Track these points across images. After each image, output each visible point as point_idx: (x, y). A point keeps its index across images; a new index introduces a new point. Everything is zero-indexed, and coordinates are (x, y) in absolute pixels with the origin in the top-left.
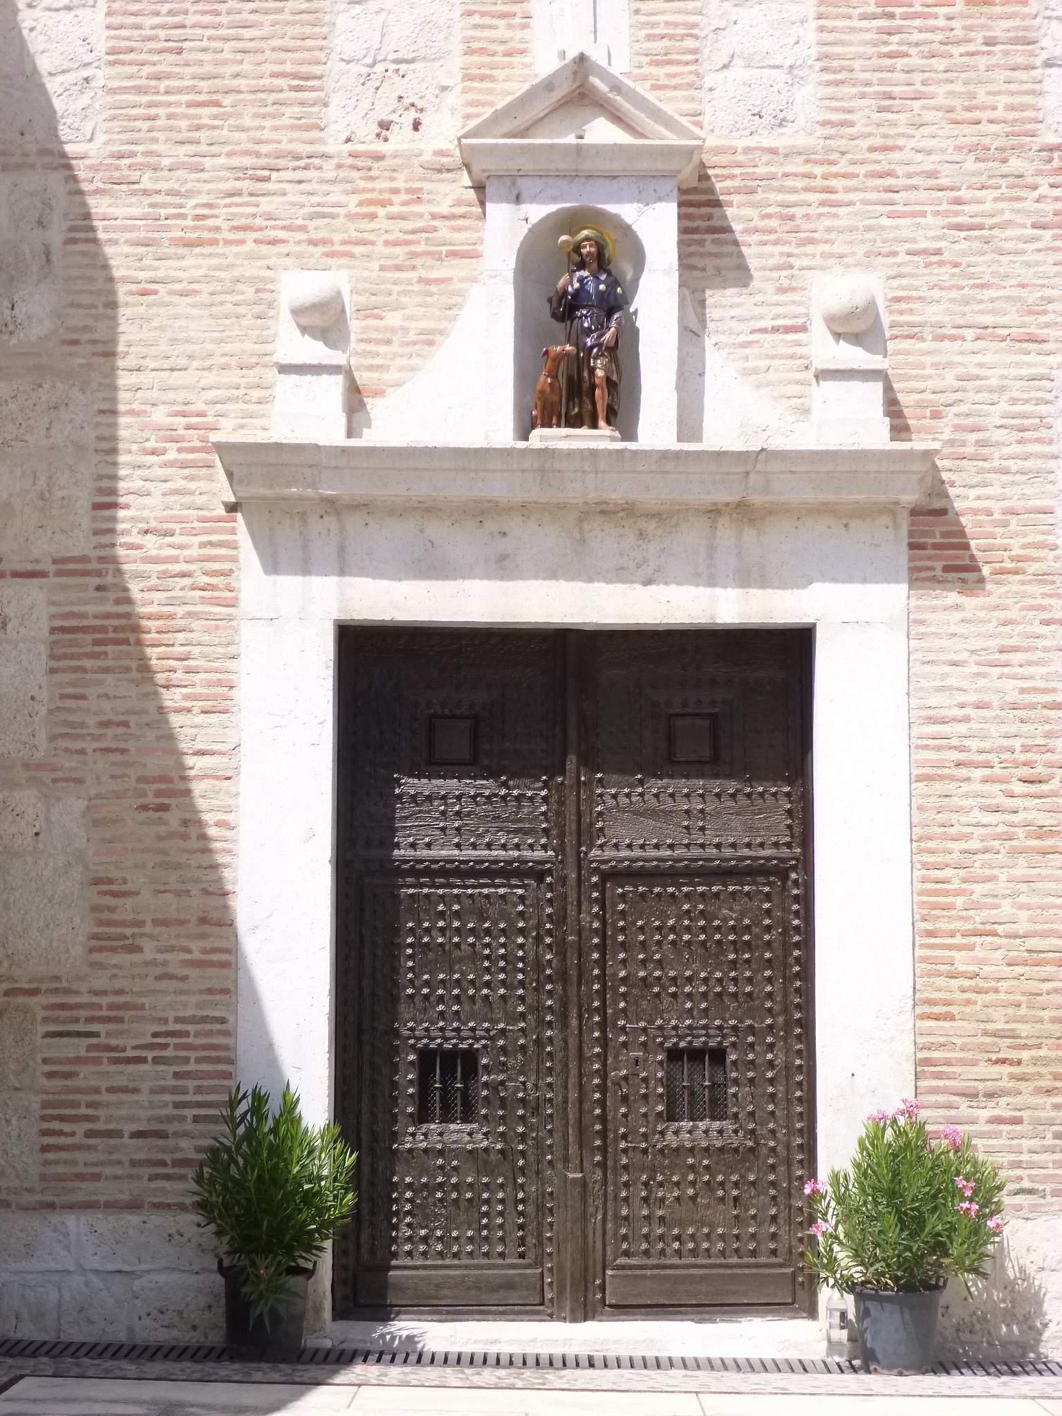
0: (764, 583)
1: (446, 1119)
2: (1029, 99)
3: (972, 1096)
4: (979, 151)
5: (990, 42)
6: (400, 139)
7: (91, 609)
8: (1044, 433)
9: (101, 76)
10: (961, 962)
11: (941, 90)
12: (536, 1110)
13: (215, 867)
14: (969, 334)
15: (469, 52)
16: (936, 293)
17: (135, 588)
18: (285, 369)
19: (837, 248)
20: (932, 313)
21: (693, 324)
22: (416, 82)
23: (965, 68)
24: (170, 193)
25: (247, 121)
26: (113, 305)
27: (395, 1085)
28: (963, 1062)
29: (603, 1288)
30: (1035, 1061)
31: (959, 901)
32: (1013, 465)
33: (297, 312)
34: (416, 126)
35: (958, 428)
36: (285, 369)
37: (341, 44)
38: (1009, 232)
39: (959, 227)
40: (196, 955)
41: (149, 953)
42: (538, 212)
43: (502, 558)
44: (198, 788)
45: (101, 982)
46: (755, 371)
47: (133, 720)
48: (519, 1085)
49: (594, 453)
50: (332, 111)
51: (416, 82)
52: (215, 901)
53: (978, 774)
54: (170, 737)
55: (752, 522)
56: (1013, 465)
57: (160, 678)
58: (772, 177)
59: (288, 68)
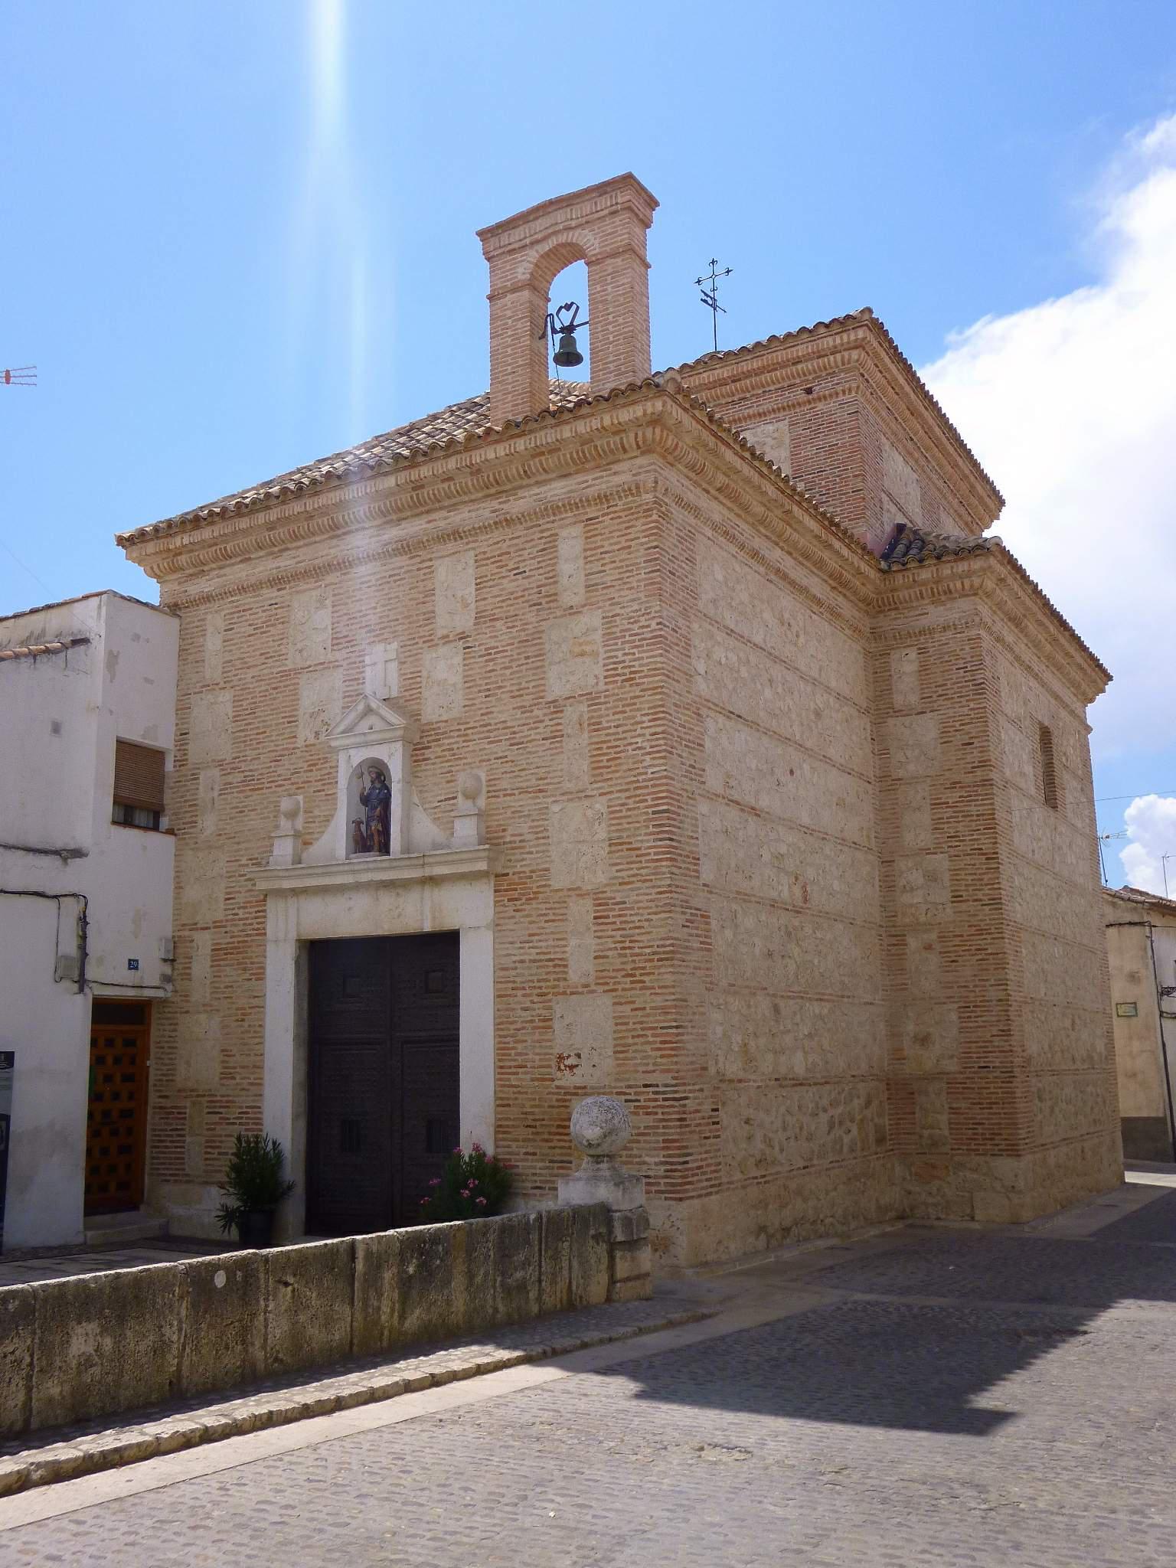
14: (516, 792)
31: (513, 1052)
35: (512, 835)
41: (238, 1081)
58: (446, 733)
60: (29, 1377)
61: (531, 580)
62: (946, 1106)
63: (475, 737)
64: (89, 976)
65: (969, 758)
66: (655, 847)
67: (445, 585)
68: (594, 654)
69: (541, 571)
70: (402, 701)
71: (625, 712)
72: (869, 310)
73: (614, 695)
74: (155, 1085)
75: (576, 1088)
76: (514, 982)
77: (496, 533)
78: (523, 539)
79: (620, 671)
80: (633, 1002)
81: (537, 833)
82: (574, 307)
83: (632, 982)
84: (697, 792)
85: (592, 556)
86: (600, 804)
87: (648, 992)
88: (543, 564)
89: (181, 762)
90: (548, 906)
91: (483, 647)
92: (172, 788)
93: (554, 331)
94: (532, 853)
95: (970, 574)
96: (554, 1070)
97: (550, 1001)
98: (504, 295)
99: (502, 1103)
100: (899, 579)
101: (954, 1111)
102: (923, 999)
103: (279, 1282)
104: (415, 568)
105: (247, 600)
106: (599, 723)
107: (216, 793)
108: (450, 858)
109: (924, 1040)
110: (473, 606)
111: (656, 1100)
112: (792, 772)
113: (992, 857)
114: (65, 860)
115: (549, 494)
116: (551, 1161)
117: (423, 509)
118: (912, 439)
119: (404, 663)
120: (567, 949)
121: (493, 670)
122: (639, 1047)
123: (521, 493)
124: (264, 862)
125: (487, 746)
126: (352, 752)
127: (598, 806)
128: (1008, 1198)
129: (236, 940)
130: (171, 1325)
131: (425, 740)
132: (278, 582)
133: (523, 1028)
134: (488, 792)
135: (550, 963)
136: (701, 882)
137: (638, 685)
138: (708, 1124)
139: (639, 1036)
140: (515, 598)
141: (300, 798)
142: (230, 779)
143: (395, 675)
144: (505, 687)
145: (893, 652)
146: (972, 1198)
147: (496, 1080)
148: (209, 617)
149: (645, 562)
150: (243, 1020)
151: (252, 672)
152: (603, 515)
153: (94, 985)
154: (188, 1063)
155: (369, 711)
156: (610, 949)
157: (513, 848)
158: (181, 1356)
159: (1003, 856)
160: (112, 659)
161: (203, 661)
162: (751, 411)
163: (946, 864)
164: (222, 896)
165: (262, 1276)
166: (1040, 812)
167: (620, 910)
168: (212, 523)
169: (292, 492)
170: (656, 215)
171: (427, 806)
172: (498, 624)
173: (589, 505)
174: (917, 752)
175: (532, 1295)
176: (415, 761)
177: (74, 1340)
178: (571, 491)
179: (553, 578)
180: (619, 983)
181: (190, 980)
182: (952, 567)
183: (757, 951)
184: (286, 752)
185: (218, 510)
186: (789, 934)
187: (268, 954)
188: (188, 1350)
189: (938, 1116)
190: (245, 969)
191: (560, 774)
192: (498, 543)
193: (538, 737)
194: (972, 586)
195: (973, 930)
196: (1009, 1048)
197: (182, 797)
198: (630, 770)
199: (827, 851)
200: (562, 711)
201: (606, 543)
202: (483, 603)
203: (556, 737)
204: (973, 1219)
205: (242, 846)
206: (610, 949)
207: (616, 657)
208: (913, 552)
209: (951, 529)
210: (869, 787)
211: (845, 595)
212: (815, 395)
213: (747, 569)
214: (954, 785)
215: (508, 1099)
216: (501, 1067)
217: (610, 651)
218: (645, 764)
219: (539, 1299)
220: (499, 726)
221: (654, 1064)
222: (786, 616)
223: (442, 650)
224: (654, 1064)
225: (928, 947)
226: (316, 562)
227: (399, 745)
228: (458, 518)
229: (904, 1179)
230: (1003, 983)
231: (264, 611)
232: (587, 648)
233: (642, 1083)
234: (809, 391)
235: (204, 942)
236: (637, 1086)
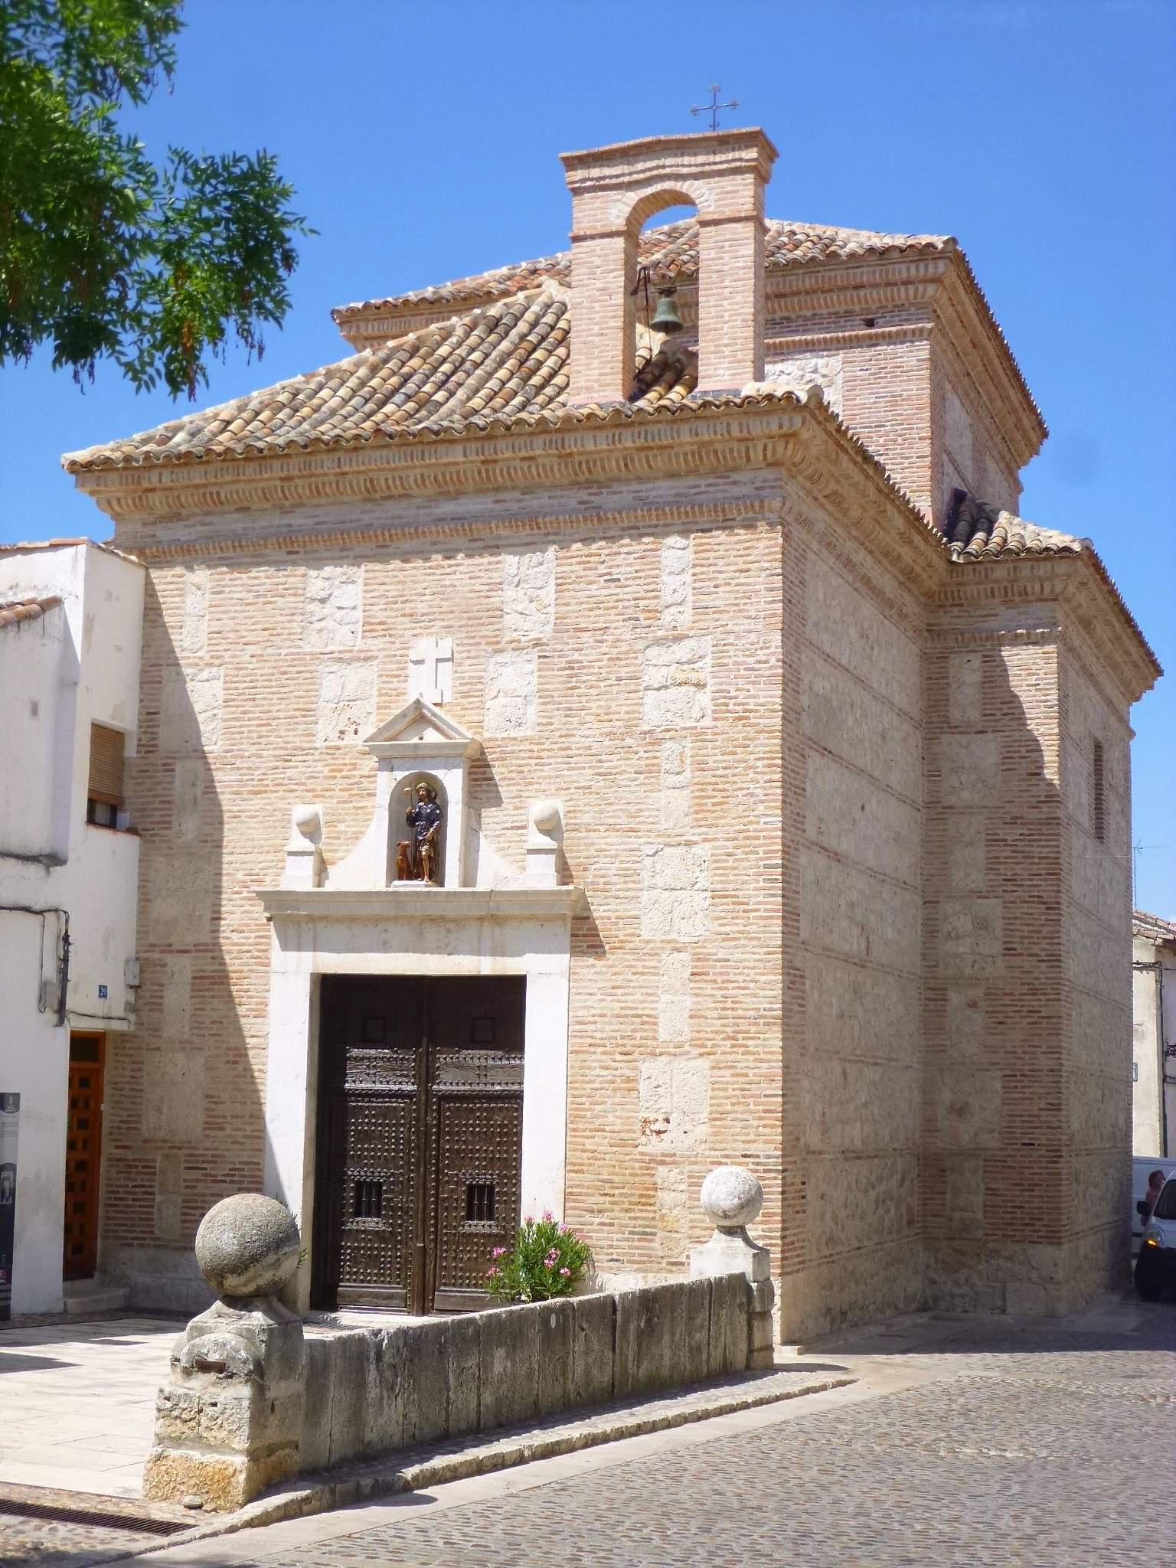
0: (503, 954)
1: (481, 1219)
2: (636, 708)
3: (592, 1211)
4: (611, 735)
5: (619, 679)
6: (349, 740)
7: (209, 968)
8: (636, 878)
9: (220, 712)
10: (589, 1144)
11: (594, 705)
12: (406, 1213)
13: (257, 1091)
14: (602, 828)
15: (380, 695)
16: (587, 808)
17: (227, 957)
18: (291, 854)
19: (543, 787)
20: (586, 818)
21: (475, 825)
22: (355, 712)
23: (607, 693)
24: (249, 769)
25: (283, 733)
26: (221, 823)
27: (344, 1198)
28: (587, 1194)
29: (433, 1300)
30: (621, 1195)
31: (588, 1114)
32: (621, 894)
33: (299, 825)
34: (356, 732)
35: (595, 876)
36: (291, 854)
37: (326, 694)
38: (624, 776)
39: (600, 774)
40: (248, 1133)
41: (228, 1131)
42: (400, 775)
43: (385, 943)
44: (251, 1053)
45: (208, 1144)
46: (502, 849)
47: (225, 1021)
48: (400, 1200)
49: (417, 893)
50: (320, 727)
51: (355, 712)
52: (256, 1107)
53: (600, 1050)
54: (239, 1029)
55: (499, 924)
56: (621, 894)
57: (237, 1000)
58: (513, 752)
59: (301, 706)
62: (982, 1187)
67: (516, 579)
69: (641, 582)
74: (111, 1134)
75: (663, 1155)
76: (592, 1037)
79: (731, 707)
85: (703, 573)
89: (148, 747)
92: (133, 778)
96: (639, 1133)
99: (572, 1167)
101: (991, 1192)
102: (963, 1064)
109: (960, 1111)
110: (552, 610)
113: (1053, 907)
114: (47, 867)
115: (654, 493)
118: (968, 374)
123: (615, 487)
128: (1046, 1290)
135: (638, 1020)
145: (952, 656)
146: (1004, 1291)
151: (251, 649)
153: (71, 1016)
154: (159, 1110)
166: (1091, 843)
174: (973, 777)
175: (704, 1357)
180: (717, 1046)
181: (161, 1011)
182: (1032, 568)
183: (834, 1012)
189: (972, 1197)
194: (1052, 590)
196: (1057, 1124)
197: (149, 790)
199: (885, 895)
201: (721, 562)
202: (565, 608)
203: (651, 770)
204: (1004, 1311)
210: (919, 814)
214: (1014, 821)
218: (756, 813)
225: (973, 1005)
229: (928, 1266)
230: (1055, 1051)
236: (735, 1157)
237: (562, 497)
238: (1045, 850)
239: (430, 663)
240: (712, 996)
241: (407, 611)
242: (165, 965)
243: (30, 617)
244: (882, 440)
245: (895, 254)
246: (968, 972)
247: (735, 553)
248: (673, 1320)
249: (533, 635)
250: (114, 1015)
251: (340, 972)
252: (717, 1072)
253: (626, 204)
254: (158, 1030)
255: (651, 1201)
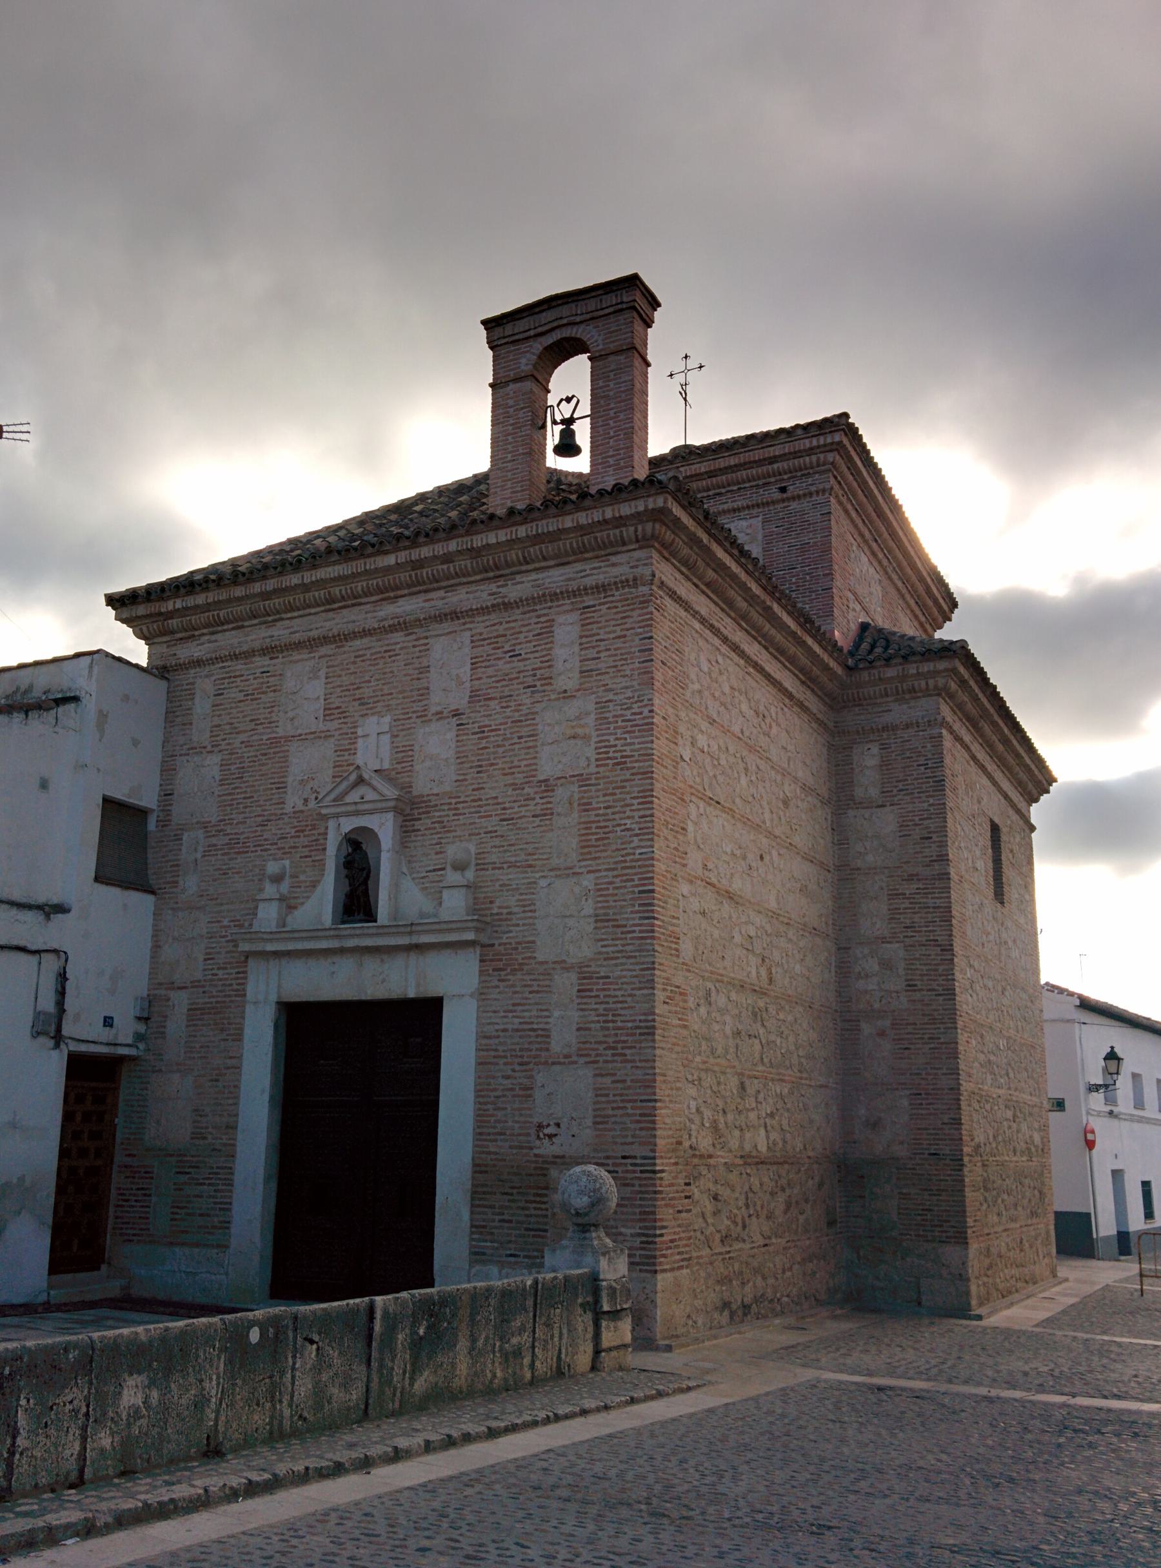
7: (201, 1001)
8: (532, 908)
16: (494, 850)
31: (493, 1119)
35: (499, 907)
38: (523, 820)
58: (436, 805)
60: (84, 1428)
61: (528, 662)
63: (466, 811)
64: (65, 1032)
65: (927, 852)
66: (640, 925)
68: (586, 738)
69: (537, 655)
70: (393, 773)
71: (614, 794)
72: (845, 415)
73: (604, 777)
76: (496, 1050)
77: (493, 616)
78: (520, 623)
79: (611, 755)
80: (615, 1075)
81: (524, 906)
82: (574, 401)
83: (613, 1055)
84: (680, 874)
86: (588, 881)
87: (629, 1065)
88: (539, 648)
89: (164, 823)
90: (532, 977)
91: (476, 725)
93: (554, 422)
94: (518, 925)
95: (935, 673)
96: (533, 1137)
97: (532, 1070)
98: (507, 383)
100: (865, 675)
103: (306, 1339)
104: (410, 644)
105: (239, 666)
106: (590, 804)
107: (199, 856)
108: (437, 927)
109: (875, 1125)
110: (468, 685)
111: (634, 1172)
112: (762, 858)
114: (48, 916)
116: (527, 1229)
117: (421, 588)
119: (397, 736)
120: (549, 1020)
121: (486, 748)
122: (618, 1119)
123: (518, 578)
124: (246, 924)
125: (477, 821)
126: (342, 820)
127: (585, 883)
129: (214, 1000)
130: (211, 1379)
131: (416, 812)
132: (270, 651)
133: (504, 1096)
134: (477, 864)
136: (681, 960)
137: (628, 769)
138: (680, 1198)
139: (618, 1108)
140: (510, 680)
141: (287, 863)
142: (214, 841)
143: (388, 747)
144: (497, 764)
147: (475, 1146)
148: (199, 681)
149: (640, 651)
150: (217, 1080)
151: (243, 737)
152: (600, 604)
154: (158, 1122)
155: (361, 781)
156: (593, 1022)
157: (501, 920)
158: (218, 1412)
159: (957, 949)
160: (102, 717)
161: (191, 724)
162: (726, 507)
163: (902, 953)
164: (201, 957)
165: (291, 1334)
167: (604, 984)
168: (207, 589)
169: (291, 564)
170: (657, 315)
171: (415, 875)
172: (492, 703)
173: (587, 594)
175: (527, 1361)
176: (405, 832)
177: (125, 1392)
178: (569, 579)
179: (549, 663)
180: (601, 1055)
181: (164, 1038)
184: (273, 817)
185: (213, 577)
186: (755, 1014)
187: (247, 1015)
188: (224, 1405)
190: (222, 1030)
191: (549, 850)
192: (494, 625)
193: (528, 814)
195: (926, 1019)
197: (163, 857)
198: (618, 850)
200: (553, 791)
201: (602, 631)
203: (547, 814)
205: (225, 907)
206: (593, 1022)
207: (608, 741)
208: (878, 650)
209: (907, 627)
211: (813, 690)
212: (788, 494)
213: (729, 661)
214: (911, 878)
215: (486, 1166)
216: (480, 1134)
217: (603, 735)
218: (632, 845)
219: (532, 1365)
220: (490, 801)
221: (633, 1136)
222: (762, 708)
223: (434, 726)
224: (633, 1136)
225: (882, 1034)
226: (311, 634)
227: (390, 815)
228: (455, 599)
231: (255, 679)
232: (580, 731)
233: (619, 1155)
234: (783, 490)
235: (181, 1001)
236: (616, 1158)
237: (477, 591)
238: (938, 901)
239: (373, 738)
240: (596, 1010)
241: (357, 697)
242: (168, 1000)
243: (40, 706)
244: (794, 580)
245: (799, 432)
246: (877, 1006)
247: (613, 623)
248: (473, 1322)
249: (453, 707)
250: (119, 1042)
251: (311, 999)
252: (599, 1079)
253: (533, 354)
254: (160, 1055)
255: (545, 1199)
